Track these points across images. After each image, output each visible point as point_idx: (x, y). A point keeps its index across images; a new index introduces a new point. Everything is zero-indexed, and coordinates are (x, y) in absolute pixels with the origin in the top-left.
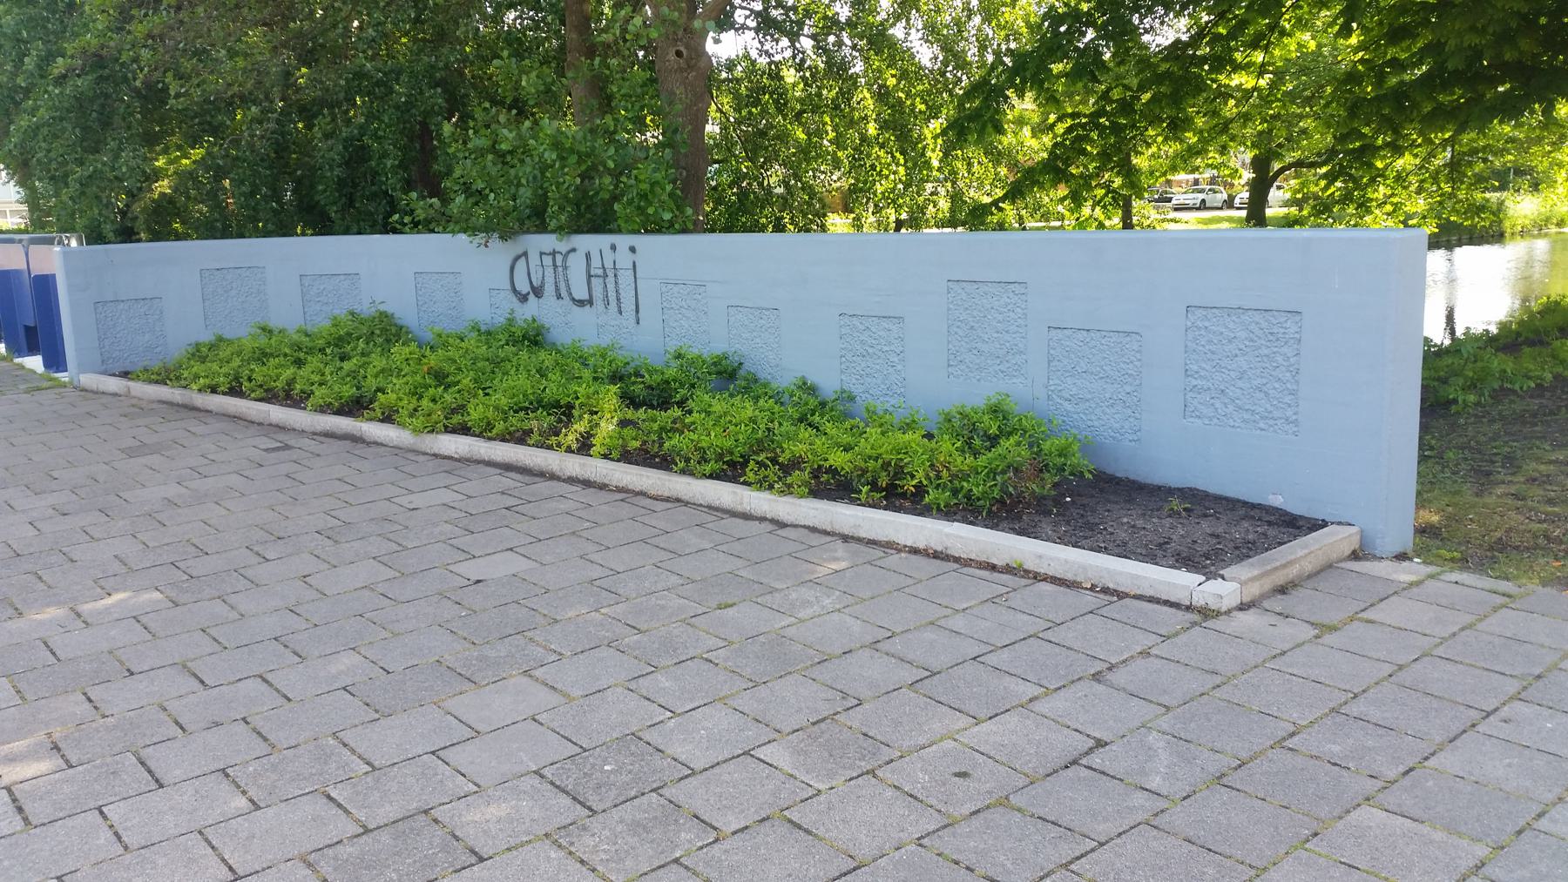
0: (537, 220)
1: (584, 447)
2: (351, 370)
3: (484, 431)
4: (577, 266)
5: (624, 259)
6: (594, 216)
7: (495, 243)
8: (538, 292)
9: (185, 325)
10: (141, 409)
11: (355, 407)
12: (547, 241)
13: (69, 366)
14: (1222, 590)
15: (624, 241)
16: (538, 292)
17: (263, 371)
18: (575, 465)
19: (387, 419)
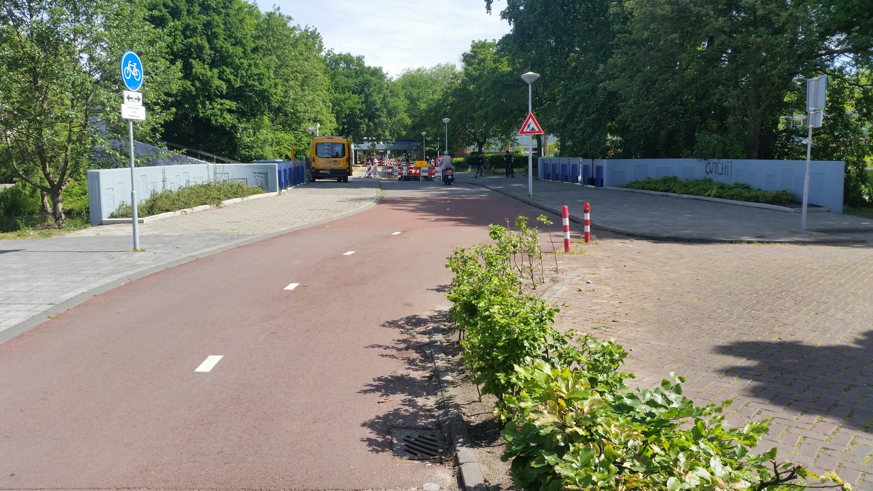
0: (713, 156)
1: (709, 195)
2: (668, 185)
3: (692, 193)
4: (720, 166)
5: (730, 164)
6: (726, 156)
7: (703, 160)
8: (711, 172)
9: (629, 178)
10: (622, 192)
11: (667, 191)
12: (715, 160)
13: (817, 162)
14: (793, 210)
15: (729, 160)
16: (711, 172)
17: (381, 201)
18: (707, 198)
19: (674, 192)
